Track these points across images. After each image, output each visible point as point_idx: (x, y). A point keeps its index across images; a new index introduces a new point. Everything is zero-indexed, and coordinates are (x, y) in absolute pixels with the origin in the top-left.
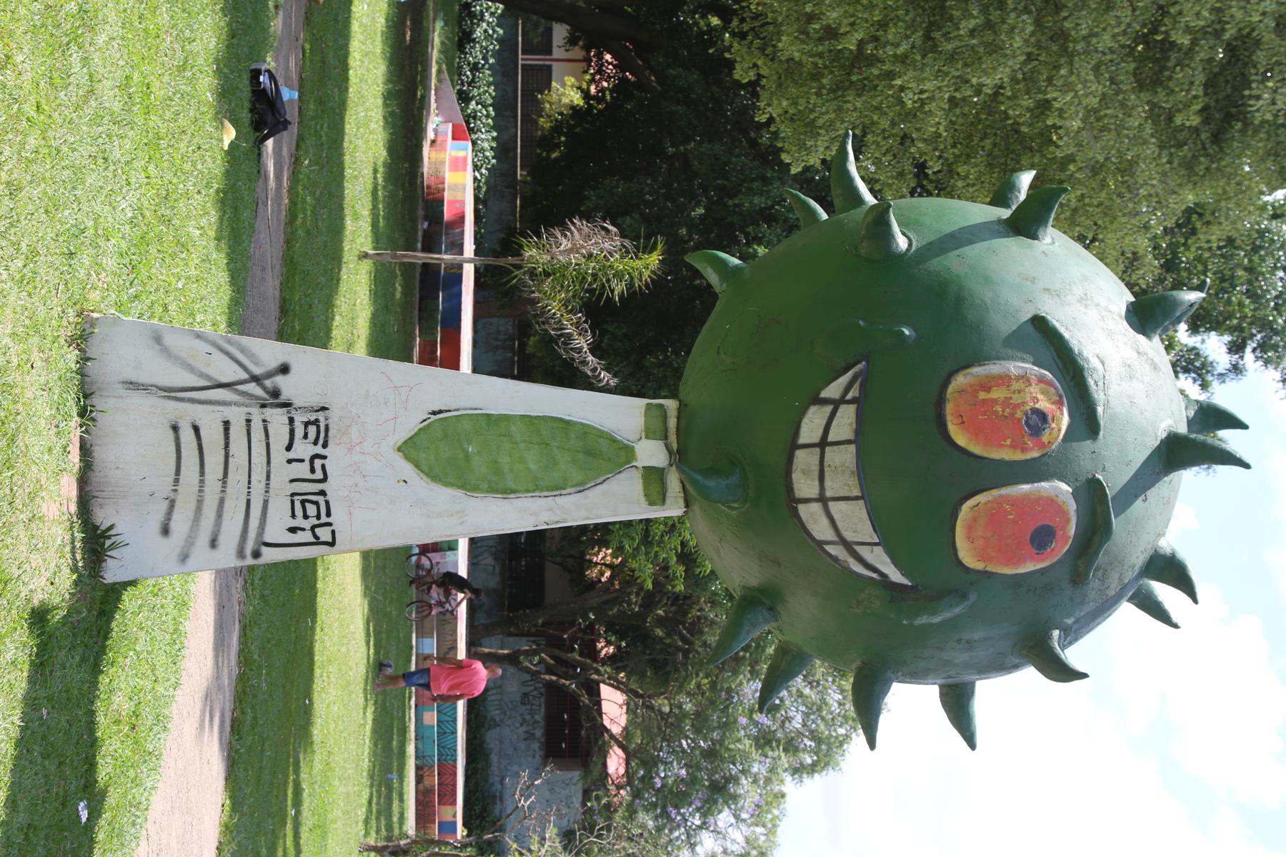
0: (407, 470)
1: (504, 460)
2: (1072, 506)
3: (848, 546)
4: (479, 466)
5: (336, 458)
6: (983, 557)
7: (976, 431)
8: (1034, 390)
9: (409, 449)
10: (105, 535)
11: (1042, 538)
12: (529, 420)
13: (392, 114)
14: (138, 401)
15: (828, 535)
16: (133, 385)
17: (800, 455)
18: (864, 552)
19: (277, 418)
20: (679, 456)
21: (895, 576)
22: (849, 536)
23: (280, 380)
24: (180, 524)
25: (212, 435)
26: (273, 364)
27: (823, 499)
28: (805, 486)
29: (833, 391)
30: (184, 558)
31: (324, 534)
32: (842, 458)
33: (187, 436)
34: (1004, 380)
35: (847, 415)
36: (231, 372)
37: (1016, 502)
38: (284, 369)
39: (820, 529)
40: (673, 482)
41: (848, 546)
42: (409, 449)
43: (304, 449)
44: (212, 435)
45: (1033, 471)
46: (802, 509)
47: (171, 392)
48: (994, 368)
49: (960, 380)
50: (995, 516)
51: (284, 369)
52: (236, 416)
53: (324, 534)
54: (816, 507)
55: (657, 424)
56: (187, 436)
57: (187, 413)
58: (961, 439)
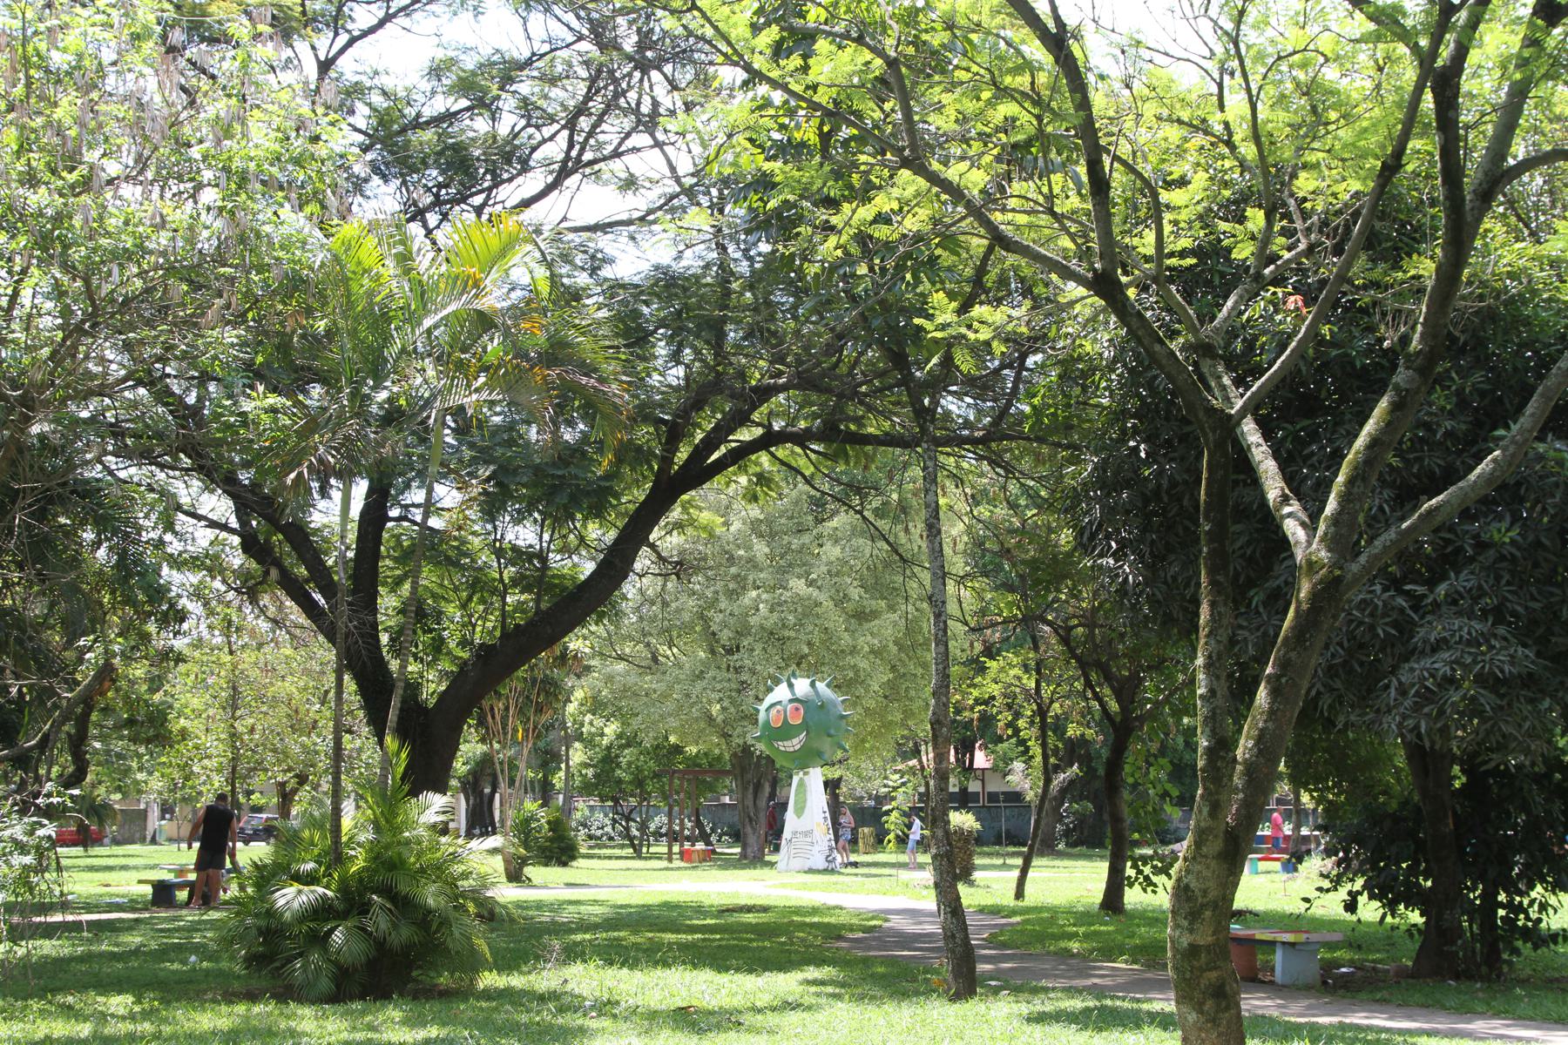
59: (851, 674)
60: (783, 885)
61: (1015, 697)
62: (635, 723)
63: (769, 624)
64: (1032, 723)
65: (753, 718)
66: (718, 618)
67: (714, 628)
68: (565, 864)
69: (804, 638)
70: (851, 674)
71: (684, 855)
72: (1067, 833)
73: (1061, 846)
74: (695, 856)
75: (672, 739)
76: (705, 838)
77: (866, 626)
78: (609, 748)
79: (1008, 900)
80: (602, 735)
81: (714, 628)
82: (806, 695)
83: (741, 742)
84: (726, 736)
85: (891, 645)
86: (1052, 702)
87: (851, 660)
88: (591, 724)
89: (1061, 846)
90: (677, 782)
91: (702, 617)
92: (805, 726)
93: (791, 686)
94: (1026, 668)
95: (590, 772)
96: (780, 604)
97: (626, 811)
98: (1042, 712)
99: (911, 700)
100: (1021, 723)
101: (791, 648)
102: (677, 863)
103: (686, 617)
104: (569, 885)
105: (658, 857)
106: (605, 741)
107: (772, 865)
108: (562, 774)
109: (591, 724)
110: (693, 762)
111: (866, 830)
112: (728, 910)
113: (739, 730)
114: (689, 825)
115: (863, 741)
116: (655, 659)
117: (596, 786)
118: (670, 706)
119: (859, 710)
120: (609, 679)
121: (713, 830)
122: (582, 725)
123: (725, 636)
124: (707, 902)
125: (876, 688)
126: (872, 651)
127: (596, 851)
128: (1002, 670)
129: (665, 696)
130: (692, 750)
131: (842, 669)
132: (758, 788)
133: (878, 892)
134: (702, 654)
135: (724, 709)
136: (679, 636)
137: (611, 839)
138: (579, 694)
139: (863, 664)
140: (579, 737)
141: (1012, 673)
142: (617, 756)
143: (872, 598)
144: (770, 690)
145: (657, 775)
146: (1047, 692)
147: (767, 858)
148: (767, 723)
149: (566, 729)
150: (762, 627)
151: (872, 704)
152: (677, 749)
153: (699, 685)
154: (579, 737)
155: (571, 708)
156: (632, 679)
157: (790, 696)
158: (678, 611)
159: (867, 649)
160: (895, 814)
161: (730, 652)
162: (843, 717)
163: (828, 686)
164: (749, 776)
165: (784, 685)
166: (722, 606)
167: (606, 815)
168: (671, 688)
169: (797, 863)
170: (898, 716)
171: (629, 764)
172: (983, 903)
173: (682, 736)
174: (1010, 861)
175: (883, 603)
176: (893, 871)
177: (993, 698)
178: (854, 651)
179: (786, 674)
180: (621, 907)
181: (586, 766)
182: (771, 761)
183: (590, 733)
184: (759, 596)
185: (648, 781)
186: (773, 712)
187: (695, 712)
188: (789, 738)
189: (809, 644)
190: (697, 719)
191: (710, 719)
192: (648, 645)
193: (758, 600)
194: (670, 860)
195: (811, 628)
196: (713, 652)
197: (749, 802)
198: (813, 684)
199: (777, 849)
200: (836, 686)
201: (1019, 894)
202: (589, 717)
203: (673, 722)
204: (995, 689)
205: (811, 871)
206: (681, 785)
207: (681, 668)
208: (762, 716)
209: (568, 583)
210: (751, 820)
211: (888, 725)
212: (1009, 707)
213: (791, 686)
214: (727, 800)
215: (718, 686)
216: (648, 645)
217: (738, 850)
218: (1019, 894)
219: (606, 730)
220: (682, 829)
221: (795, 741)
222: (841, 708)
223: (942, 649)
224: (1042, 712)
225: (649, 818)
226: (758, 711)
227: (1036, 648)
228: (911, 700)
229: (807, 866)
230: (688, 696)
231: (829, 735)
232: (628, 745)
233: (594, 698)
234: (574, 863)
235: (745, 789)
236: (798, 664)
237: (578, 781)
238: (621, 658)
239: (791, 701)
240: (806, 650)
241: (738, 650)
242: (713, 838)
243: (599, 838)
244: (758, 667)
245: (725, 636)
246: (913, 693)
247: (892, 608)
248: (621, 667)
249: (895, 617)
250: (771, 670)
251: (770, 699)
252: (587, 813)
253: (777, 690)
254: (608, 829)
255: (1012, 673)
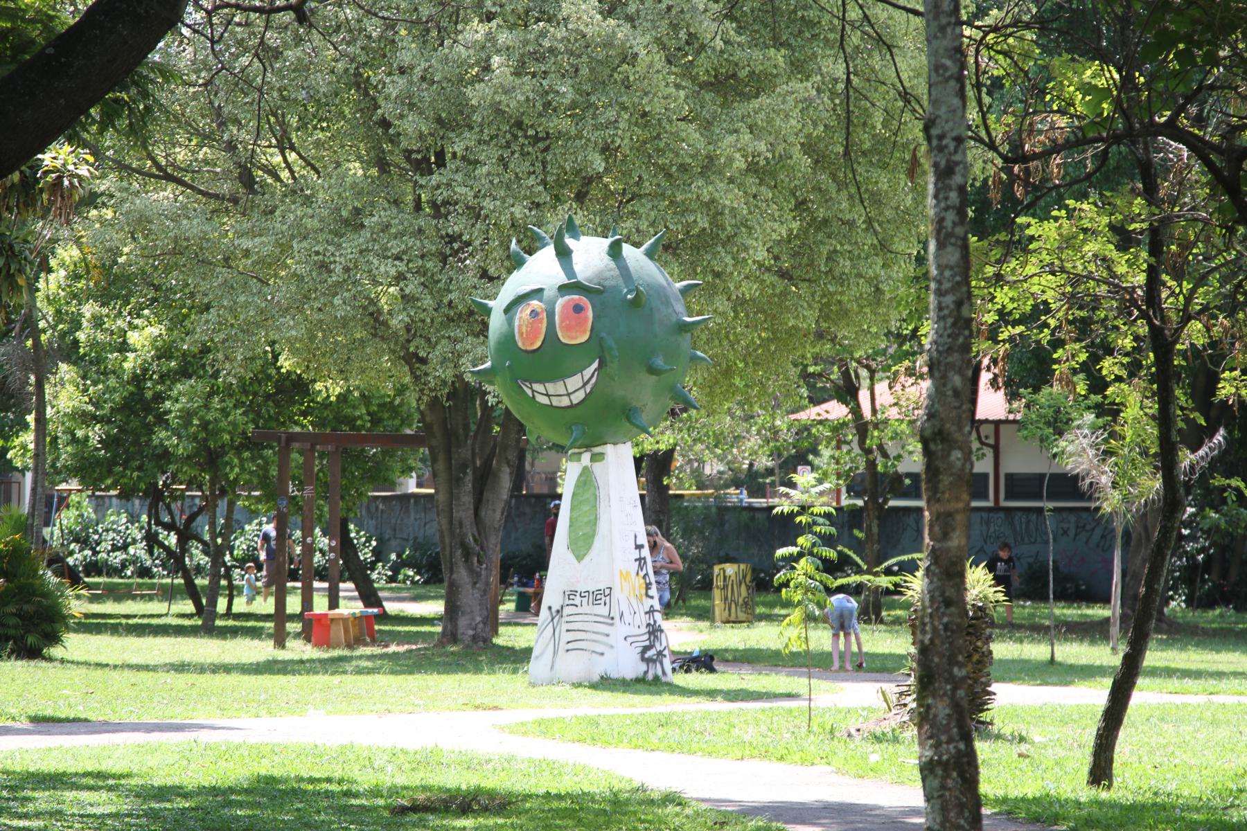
0: (587, 559)
1: (586, 520)
2: (567, 297)
3: (585, 385)
4: (587, 530)
5: (581, 588)
6: (585, 332)
7: (536, 338)
8: (524, 315)
9: (580, 558)
10: (602, 677)
11: (578, 309)
12: (572, 509)
13: (1197, 645)
14: (557, 666)
15: (582, 391)
16: (552, 668)
17: (555, 404)
18: (586, 379)
19: (567, 611)
20: (588, 447)
21: (595, 365)
22: (581, 384)
23: (554, 610)
24: (600, 649)
25: (571, 636)
26: (548, 612)
27: (569, 395)
28: (565, 402)
29: (529, 392)
30: (612, 647)
31: (607, 592)
32: (551, 387)
33: (570, 646)
34: (520, 326)
35: (537, 387)
36: (550, 628)
37: (562, 321)
38: (550, 608)
39: (580, 395)
40: (597, 450)
41: (585, 385)
42: (580, 558)
43: (578, 600)
44: (571, 636)
45: (551, 314)
46: (575, 402)
47: (555, 653)
48: (516, 331)
49: (520, 344)
50: (568, 329)
51: (550, 608)
52: (565, 627)
53: (607, 592)
54: (572, 397)
55: (576, 457)
56: (570, 646)
57: (563, 646)
58: (538, 344)
59: (704, 223)
60: (544, 728)
61: (1096, 303)
62: (203, 328)
63: (511, 104)
64: (1134, 369)
65: (476, 320)
66: (395, 86)
67: (386, 109)
68: (33, 653)
69: (595, 136)
70: (704, 223)
71: (314, 629)
72: (1191, 575)
73: (1176, 605)
74: (338, 632)
75: (286, 363)
76: (359, 575)
77: (740, 109)
78: (138, 379)
79: (1081, 791)
80: (124, 347)
81: (386, 109)
82: (600, 276)
83: (448, 374)
84: (414, 361)
85: (796, 152)
86: (1187, 318)
87: (702, 189)
88: (98, 322)
89: (1176, 605)
90: (296, 458)
91: (359, 83)
92: (597, 348)
93: (564, 254)
94: (1124, 240)
95: (95, 434)
96: (539, 57)
97: (180, 521)
98: (1161, 341)
99: (841, 280)
100: (1109, 366)
101: (564, 160)
102: (298, 649)
103: (321, 82)
104: (44, 723)
105: (245, 627)
106: (130, 363)
107: (519, 657)
108: (28, 438)
109: (98, 322)
110: (336, 413)
111: (731, 569)
112: (415, 808)
113: (443, 348)
114: (323, 542)
115: (728, 373)
116: (247, 179)
117: (107, 467)
118: (282, 291)
119: (722, 304)
120: (140, 224)
121: (379, 555)
122: (78, 326)
123: (412, 126)
124: (365, 780)
125: (762, 255)
126: (752, 168)
127: (109, 607)
128: (1068, 242)
129: (271, 263)
130: (329, 388)
131: (681, 209)
132: (484, 479)
133: (764, 755)
134: (356, 169)
135: (406, 298)
136: (302, 126)
137: (144, 572)
138: (68, 254)
139: (731, 199)
140: (70, 352)
141: (1091, 248)
142: (159, 398)
143: (753, 44)
144: (518, 263)
145: (252, 444)
146: (1172, 294)
147: (508, 636)
148: (508, 340)
149: (36, 333)
150: (498, 110)
151: (750, 290)
152: (296, 387)
153: (351, 245)
154: (70, 352)
155: (52, 284)
156: (193, 227)
157: (562, 279)
158: (301, 68)
159: (740, 163)
160: (804, 564)
161: (423, 167)
162: (684, 328)
163: (650, 254)
164: (465, 453)
165: (547, 254)
166: (405, 57)
167: (133, 519)
168: (285, 248)
169: (574, 665)
170: (808, 319)
171: (187, 416)
172: (1015, 793)
173: (307, 351)
174: (1073, 652)
175: (779, 57)
176: (797, 683)
177: (1046, 308)
178: (709, 166)
179: (555, 220)
180: (163, 793)
181: (86, 418)
182: (514, 426)
183: (93, 344)
184: (490, 37)
185: (231, 457)
186: (523, 313)
187: (340, 306)
188: (559, 374)
189: (607, 150)
190: (345, 323)
191: (375, 319)
192: (231, 147)
193: (488, 46)
194: (280, 639)
195: (611, 114)
196: (382, 164)
197: (464, 512)
198: (615, 251)
199: (529, 604)
200: (665, 250)
201: (1101, 771)
202: (89, 309)
203: (292, 328)
204: (1047, 287)
205: (606, 683)
206: (308, 465)
207: (308, 201)
208: (496, 322)
209: (35, 32)
210: (467, 554)
211: (783, 338)
212: (1083, 328)
213: (564, 254)
214: (411, 486)
215: (395, 247)
216: (231, 147)
217: (435, 607)
218: (1101, 771)
219: (133, 338)
220: (309, 550)
221: (574, 382)
222: (679, 307)
223: (953, 256)
224: (1161, 341)
225: (232, 526)
226: (488, 311)
227: (1150, 193)
228: (841, 280)
229: (599, 667)
230: (324, 267)
231: (652, 370)
232: (184, 373)
233: (106, 269)
234: (57, 651)
235: (454, 482)
236: (580, 197)
237: (66, 453)
238: (166, 175)
239: (564, 289)
240: (599, 164)
241: (441, 162)
242: (378, 576)
243: (118, 571)
244: (488, 204)
245: (412, 126)
246: (845, 265)
247: (799, 68)
248: (166, 195)
249: (805, 88)
250: (518, 211)
251: (516, 284)
252: (89, 512)
253: (532, 261)
254: (138, 550)
255: (1091, 248)
